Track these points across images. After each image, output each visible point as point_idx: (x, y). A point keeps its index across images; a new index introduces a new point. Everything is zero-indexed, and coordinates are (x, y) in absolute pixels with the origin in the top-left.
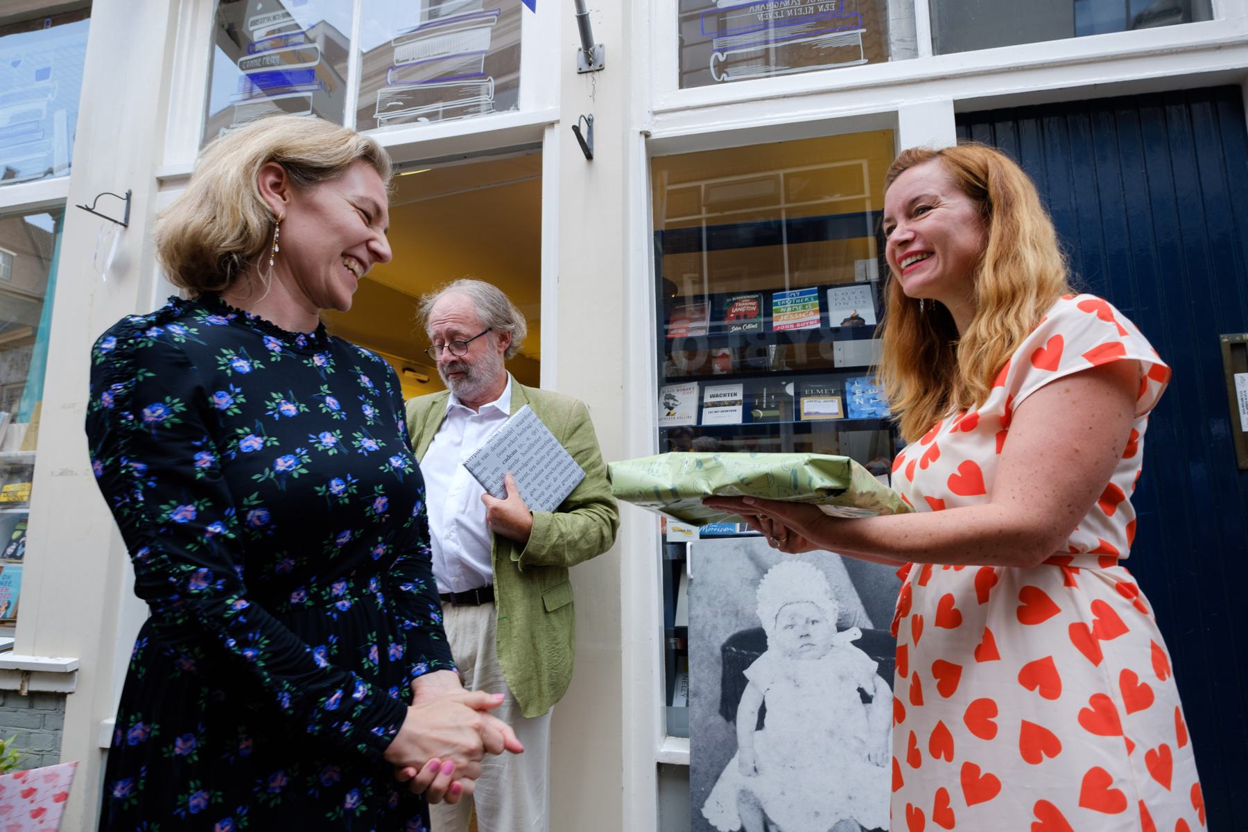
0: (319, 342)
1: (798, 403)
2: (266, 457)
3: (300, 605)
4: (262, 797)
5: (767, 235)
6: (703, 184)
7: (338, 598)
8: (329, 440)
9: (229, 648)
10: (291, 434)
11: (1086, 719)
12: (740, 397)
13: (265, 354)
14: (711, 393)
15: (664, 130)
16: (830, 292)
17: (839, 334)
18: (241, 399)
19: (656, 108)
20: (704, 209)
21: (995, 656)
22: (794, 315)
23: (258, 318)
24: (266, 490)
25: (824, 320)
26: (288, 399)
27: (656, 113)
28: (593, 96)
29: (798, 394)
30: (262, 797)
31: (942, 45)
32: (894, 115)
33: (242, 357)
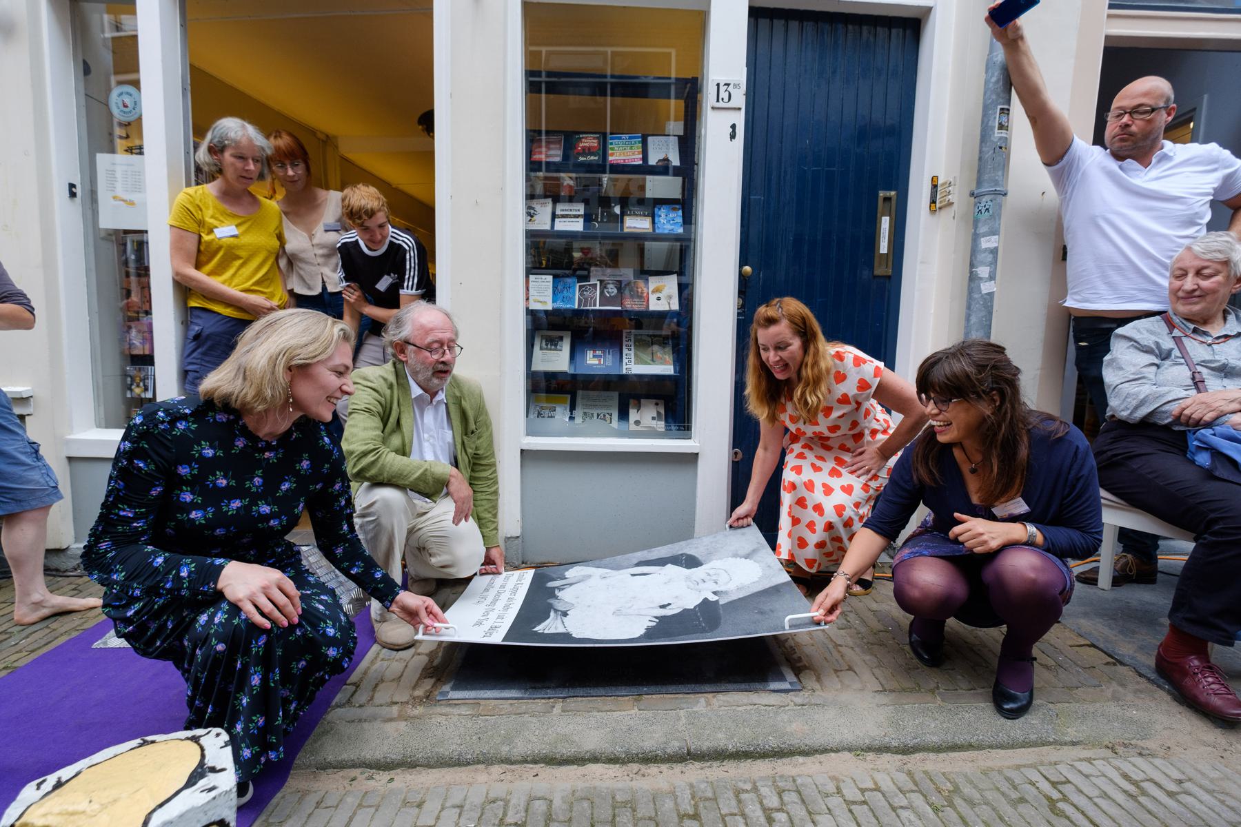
1: (622, 222)
4: (225, 509)
6: (544, 49)
9: (877, 195)
10: (214, 497)
12: (582, 212)
14: (561, 208)
16: (650, 139)
17: (654, 171)
21: (836, 507)
22: (623, 152)
25: (645, 158)
29: (623, 214)
30: (225, 509)
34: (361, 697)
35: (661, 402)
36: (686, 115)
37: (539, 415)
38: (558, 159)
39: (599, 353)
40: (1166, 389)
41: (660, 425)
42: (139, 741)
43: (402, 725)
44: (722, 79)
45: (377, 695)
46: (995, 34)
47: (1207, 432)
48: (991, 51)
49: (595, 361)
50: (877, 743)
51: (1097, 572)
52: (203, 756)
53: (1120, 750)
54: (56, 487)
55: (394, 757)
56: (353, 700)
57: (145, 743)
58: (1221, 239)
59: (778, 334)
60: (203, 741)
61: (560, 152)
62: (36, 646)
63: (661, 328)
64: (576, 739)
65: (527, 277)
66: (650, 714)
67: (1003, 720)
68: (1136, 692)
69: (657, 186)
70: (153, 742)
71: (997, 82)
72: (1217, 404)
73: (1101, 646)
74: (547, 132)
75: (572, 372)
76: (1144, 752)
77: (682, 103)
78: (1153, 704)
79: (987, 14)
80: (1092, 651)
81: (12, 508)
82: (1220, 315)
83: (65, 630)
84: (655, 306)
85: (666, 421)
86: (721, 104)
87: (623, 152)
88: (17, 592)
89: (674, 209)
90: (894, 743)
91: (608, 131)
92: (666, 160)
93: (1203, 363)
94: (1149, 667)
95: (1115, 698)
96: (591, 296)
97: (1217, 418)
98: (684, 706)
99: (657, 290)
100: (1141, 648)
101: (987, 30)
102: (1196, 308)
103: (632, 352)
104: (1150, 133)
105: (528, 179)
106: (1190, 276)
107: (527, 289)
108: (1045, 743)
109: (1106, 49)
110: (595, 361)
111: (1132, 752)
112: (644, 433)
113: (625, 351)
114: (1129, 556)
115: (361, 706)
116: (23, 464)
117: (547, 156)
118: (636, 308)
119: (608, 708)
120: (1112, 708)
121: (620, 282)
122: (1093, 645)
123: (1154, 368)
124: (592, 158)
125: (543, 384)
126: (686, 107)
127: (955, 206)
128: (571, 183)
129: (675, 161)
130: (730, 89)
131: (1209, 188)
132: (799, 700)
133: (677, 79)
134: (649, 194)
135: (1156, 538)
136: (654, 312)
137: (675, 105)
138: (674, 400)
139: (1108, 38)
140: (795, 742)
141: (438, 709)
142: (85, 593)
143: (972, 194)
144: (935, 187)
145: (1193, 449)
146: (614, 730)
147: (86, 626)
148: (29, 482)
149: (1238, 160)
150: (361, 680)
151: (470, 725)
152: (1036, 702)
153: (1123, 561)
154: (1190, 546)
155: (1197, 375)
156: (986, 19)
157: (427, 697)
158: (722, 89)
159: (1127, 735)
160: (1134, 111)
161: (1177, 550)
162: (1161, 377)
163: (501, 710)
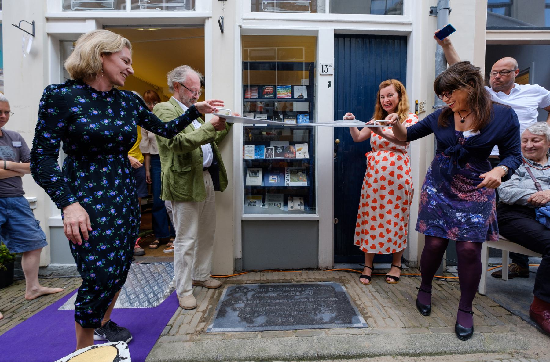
0: (110, 94)
2: (87, 124)
3: (100, 159)
5: (272, 66)
6: (249, 49)
7: (110, 158)
8: (106, 121)
10: (95, 119)
11: (372, 219)
13: (91, 98)
15: (247, 26)
16: (295, 87)
18: (81, 109)
19: (244, 17)
20: (249, 58)
22: (283, 93)
23: (91, 87)
24: (88, 131)
26: (96, 110)
27: (244, 19)
28: (223, 10)
31: (332, 11)
32: (317, 31)
33: (83, 98)
34: (173, 331)
35: (302, 198)
36: (309, 76)
37: (249, 204)
38: (256, 97)
39: (274, 177)
40: (523, 190)
41: (302, 208)
42: (91, 347)
43: (191, 344)
44: (324, 64)
45: (180, 330)
46: (438, 42)
47: (543, 209)
48: (437, 49)
49: (273, 181)
50: (402, 352)
51: (501, 272)
52: (118, 352)
53: (515, 355)
54: (45, 240)
55: (188, 358)
56: (170, 333)
57: (93, 348)
58: (543, 124)
59: (388, 90)
60: (117, 346)
61: (257, 94)
62: (34, 309)
63: (301, 166)
64: (268, 350)
65: (244, 146)
66: (300, 338)
67: (460, 341)
68: (521, 327)
69: (298, 107)
70: (97, 347)
71: (441, 61)
72: (547, 196)
73: (505, 306)
74: (251, 86)
75: (263, 186)
76: (526, 356)
77: (308, 72)
78: (529, 334)
79: (434, 35)
80: (500, 309)
81: (27, 249)
82: (545, 157)
83: (47, 302)
84: (298, 156)
85: (304, 205)
86: (324, 73)
87: (283, 93)
88: (27, 286)
89: (306, 116)
90: (411, 352)
91: (277, 84)
92: (302, 96)
93: (539, 178)
94: (527, 316)
95: (512, 331)
96: (271, 153)
97: (548, 202)
98: (316, 334)
99: (299, 150)
100: (523, 307)
101: (435, 41)
102: (534, 155)
103: (289, 177)
104: (509, 81)
105: (244, 105)
106: (529, 142)
107: (244, 151)
108: (480, 352)
109: (487, 46)
110: (273, 181)
111: (521, 356)
112: (293, 211)
113: (286, 176)
114: (516, 265)
115: (173, 335)
116: (32, 230)
117: (251, 96)
118: (290, 158)
119: (282, 336)
120: (511, 335)
121: (283, 147)
122: (500, 306)
123: (518, 181)
124: (271, 96)
125: (250, 191)
126: (310, 74)
127: (426, 112)
128: (262, 105)
129: (306, 96)
130: (328, 67)
131: (536, 103)
132: (367, 332)
133: (305, 63)
134: (295, 110)
135: (527, 256)
136: (298, 159)
137: (305, 73)
138: (307, 196)
139: (487, 41)
140: (366, 351)
141: (207, 336)
142: (54, 286)
143: (433, 107)
144: (417, 104)
145: (538, 216)
146: (285, 346)
147: (55, 300)
148: (35, 238)
149: (549, 91)
150: (173, 323)
151: (221, 343)
152: (475, 332)
153: (513, 267)
154: (540, 259)
155: (537, 184)
156: (434, 37)
157: (202, 331)
158: (324, 67)
159: (518, 348)
160: (501, 72)
161: (535, 262)
162: (521, 185)
163: (235, 336)
